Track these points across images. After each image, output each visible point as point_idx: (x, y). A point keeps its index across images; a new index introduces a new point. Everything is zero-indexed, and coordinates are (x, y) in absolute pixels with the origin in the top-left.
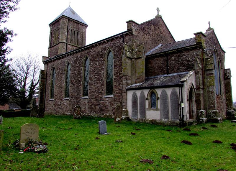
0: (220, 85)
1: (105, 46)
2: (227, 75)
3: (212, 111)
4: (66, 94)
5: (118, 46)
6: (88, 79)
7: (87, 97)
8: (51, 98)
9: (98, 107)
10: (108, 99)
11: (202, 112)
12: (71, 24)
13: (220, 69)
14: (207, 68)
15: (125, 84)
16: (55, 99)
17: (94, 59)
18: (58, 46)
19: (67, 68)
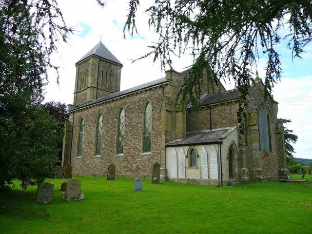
0: (270, 141)
1: (143, 96)
2: (279, 129)
3: (255, 170)
4: (96, 150)
5: (157, 98)
6: (123, 133)
7: (122, 154)
8: (78, 155)
9: (134, 166)
10: (145, 157)
11: (244, 170)
12: (103, 64)
13: (270, 122)
14: (251, 124)
15: (164, 140)
16: (83, 157)
17: (129, 111)
18: (86, 91)
19: (99, 120)
